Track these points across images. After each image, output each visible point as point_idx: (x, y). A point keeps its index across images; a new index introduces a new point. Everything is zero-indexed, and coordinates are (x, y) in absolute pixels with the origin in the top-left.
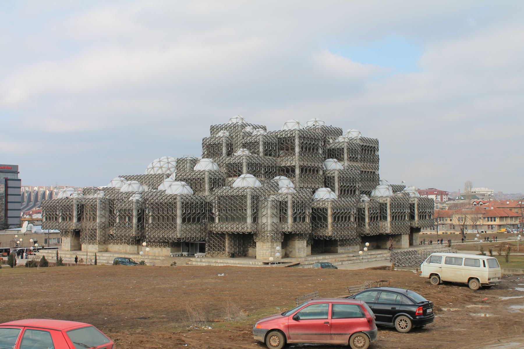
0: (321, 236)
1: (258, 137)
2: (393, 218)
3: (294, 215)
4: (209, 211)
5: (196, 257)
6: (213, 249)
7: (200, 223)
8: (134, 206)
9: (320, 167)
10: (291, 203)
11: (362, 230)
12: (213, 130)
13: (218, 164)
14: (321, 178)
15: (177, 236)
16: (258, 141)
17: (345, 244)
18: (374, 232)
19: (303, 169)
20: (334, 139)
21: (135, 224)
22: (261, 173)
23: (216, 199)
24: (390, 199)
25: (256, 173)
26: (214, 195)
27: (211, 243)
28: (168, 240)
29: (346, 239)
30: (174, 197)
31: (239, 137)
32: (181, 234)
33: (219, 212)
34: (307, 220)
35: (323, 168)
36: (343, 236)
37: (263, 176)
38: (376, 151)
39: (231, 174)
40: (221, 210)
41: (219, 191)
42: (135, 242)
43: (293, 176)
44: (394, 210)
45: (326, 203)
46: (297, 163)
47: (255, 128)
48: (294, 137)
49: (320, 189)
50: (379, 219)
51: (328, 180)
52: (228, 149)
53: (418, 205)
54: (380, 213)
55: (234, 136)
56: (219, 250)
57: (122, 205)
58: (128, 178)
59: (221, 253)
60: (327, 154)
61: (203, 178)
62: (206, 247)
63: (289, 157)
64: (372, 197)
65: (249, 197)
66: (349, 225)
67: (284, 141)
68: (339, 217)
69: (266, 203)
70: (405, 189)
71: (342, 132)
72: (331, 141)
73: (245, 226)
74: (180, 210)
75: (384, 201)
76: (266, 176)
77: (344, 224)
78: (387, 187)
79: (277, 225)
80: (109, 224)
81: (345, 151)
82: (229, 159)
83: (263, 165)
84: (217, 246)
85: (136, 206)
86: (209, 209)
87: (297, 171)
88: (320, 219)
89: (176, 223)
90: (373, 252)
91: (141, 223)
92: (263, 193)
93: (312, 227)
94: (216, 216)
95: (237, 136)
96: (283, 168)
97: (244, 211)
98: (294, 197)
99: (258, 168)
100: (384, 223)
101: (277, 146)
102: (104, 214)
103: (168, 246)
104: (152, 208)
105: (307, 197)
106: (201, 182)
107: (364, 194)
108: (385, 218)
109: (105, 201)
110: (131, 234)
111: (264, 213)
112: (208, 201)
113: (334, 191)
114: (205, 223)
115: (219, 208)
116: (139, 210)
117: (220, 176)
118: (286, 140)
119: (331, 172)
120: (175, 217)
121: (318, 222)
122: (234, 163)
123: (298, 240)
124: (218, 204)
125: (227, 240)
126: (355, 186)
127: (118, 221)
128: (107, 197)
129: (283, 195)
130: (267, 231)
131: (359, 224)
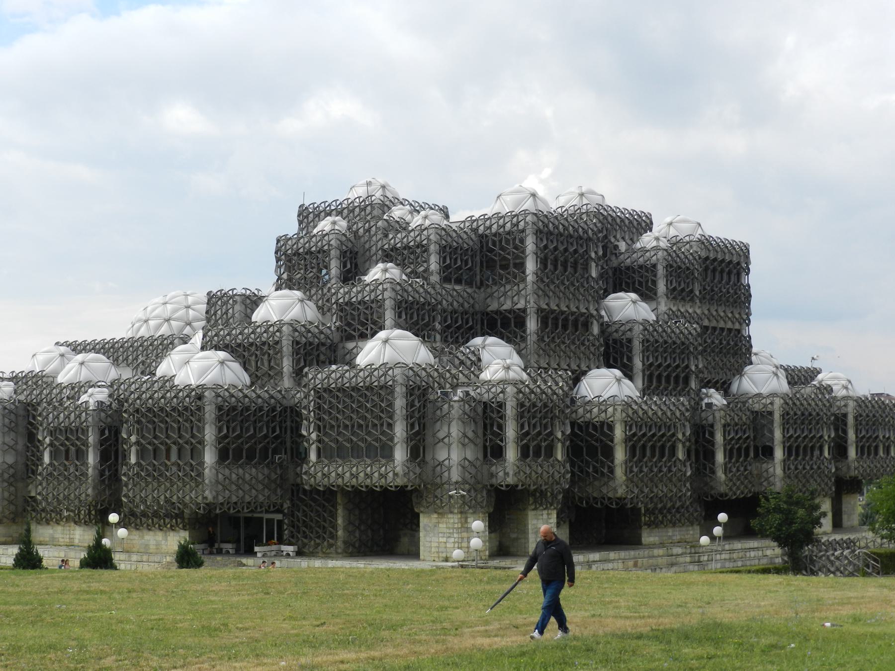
0: (595, 498)
1: (425, 232)
2: (789, 451)
3: (521, 442)
4: (292, 432)
5: (259, 555)
6: (304, 532)
7: (268, 463)
8: (90, 419)
9: (592, 316)
10: (515, 406)
11: (706, 484)
12: (307, 217)
13: (318, 307)
14: (597, 344)
15: (206, 498)
16: (425, 242)
17: (662, 522)
18: (738, 488)
19: (546, 318)
20: (630, 242)
21: (95, 468)
22: (434, 329)
23: (311, 398)
24: (782, 401)
25: (420, 330)
26: (305, 386)
27: (298, 516)
28: (179, 509)
29: (664, 507)
30: (198, 394)
31: (375, 234)
32: (216, 491)
33: (319, 431)
34: (559, 455)
35: (602, 317)
36: (655, 500)
37: (438, 337)
38: (743, 274)
39: (352, 332)
40: (325, 427)
41: (319, 376)
42: (96, 515)
43: (518, 337)
44: (791, 432)
45: (611, 410)
46: (532, 301)
47: (416, 209)
48: (523, 231)
49: (594, 372)
50: (752, 454)
51: (614, 348)
52: (345, 266)
53: (856, 418)
54: (755, 437)
55: (361, 230)
56: (318, 537)
57: (57, 417)
58: (77, 348)
59: (325, 543)
60: (611, 281)
61: (277, 343)
62: (285, 527)
63: (508, 287)
64: (734, 396)
65: (399, 390)
66: (674, 469)
67: (494, 244)
68: (644, 447)
69: (446, 406)
70: (820, 377)
71: (652, 223)
72: (623, 246)
73: (389, 469)
74: (214, 427)
75: (765, 406)
76: (446, 337)
77: (659, 465)
78: (774, 369)
79: (476, 468)
80: (28, 470)
81: (661, 271)
82: (346, 290)
83: (439, 306)
84: (313, 525)
85: (97, 419)
86: (294, 425)
87: (532, 325)
88: (592, 451)
89: (201, 464)
90: (738, 545)
91: (110, 465)
92: (437, 379)
93: (573, 474)
94: (311, 442)
95: (369, 230)
96: (494, 315)
97: (385, 428)
98: (523, 390)
99: (424, 314)
100: (765, 465)
101: (478, 257)
102: (12, 443)
103: (181, 526)
104: (139, 422)
105: (557, 391)
106: (271, 352)
107: (710, 388)
108: (768, 452)
109: (17, 407)
110: (84, 495)
111: (441, 435)
112: (292, 403)
113: (630, 378)
114: (282, 462)
115: (318, 422)
116: (104, 429)
117: (322, 336)
118: (501, 241)
119: (622, 328)
120: (199, 446)
121: (587, 461)
122: (359, 303)
123: (533, 507)
124: (317, 411)
125: (340, 512)
126: (687, 367)
127: (47, 459)
128: (22, 397)
129: (494, 386)
130: (448, 482)
131: (698, 469)
